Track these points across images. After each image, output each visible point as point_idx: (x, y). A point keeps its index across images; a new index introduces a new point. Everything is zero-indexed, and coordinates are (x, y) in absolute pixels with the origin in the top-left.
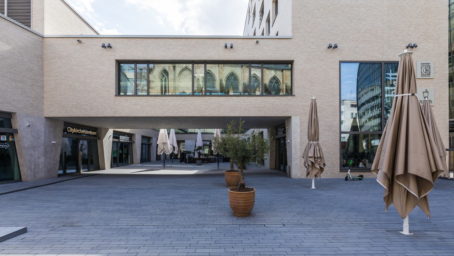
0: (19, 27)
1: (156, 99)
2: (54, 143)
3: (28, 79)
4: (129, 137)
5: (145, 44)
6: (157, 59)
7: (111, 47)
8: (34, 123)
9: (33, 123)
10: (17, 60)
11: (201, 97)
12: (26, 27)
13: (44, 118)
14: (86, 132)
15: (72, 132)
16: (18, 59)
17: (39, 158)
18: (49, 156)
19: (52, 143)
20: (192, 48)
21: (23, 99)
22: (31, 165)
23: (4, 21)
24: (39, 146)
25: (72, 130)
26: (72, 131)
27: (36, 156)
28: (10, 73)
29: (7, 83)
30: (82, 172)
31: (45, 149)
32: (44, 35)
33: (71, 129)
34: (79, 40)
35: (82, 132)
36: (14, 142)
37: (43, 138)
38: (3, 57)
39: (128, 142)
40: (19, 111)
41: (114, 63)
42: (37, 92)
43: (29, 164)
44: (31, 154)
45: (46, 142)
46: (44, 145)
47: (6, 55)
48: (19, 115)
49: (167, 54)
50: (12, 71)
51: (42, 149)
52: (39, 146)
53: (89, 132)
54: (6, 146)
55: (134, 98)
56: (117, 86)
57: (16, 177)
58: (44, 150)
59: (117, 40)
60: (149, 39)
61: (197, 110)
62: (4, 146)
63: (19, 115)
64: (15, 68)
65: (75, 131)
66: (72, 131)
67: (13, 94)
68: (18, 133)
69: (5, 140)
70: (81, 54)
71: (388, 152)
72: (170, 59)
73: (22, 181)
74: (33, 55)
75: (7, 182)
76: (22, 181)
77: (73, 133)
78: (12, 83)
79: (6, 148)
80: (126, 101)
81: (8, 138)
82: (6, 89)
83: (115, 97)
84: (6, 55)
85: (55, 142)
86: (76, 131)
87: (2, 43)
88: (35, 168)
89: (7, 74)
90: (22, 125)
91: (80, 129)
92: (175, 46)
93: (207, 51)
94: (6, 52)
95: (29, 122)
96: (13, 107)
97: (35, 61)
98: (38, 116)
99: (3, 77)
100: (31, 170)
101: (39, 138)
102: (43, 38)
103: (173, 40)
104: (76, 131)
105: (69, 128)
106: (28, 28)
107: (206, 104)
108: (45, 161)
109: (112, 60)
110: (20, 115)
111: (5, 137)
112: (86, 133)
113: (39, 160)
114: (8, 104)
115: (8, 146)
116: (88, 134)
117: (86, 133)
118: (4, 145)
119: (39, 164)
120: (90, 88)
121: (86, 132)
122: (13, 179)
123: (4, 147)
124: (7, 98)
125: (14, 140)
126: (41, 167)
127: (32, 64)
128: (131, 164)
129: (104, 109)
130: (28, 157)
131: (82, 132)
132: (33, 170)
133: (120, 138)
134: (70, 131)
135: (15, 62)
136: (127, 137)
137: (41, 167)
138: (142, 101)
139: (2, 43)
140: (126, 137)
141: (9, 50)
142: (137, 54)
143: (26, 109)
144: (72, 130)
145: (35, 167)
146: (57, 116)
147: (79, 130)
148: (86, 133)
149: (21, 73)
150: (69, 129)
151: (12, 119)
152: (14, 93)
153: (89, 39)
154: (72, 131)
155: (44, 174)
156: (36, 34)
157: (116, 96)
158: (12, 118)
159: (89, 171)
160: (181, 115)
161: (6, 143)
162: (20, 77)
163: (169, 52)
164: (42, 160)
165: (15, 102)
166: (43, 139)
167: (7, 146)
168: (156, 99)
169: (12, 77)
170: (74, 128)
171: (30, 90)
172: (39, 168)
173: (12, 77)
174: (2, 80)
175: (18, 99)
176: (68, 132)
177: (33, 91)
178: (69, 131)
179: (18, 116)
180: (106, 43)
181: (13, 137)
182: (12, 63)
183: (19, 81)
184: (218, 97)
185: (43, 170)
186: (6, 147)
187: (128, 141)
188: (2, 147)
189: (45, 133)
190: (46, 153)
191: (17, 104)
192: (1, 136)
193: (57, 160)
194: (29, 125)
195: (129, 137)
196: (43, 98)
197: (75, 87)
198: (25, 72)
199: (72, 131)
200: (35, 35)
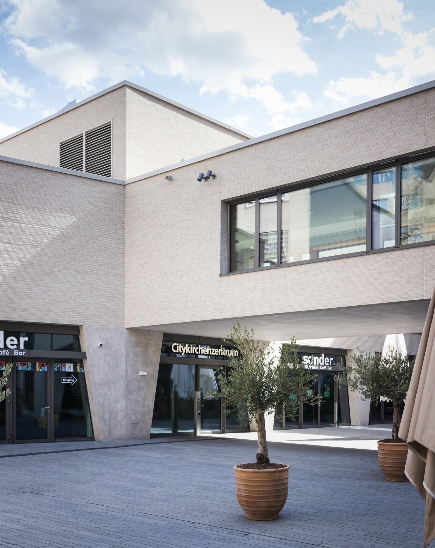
0: (87, 179)
1: (289, 272)
2: (144, 376)
3: (100, 266)
4: (331, 359)
5: (270, 153)
6: (292, 182)
7: (214, 176)
8: (109, 340)
9: (107, 341)
10: (84, 236)
11: (380, 254)
12: (101, 177)
13: (125, 330)
14: (212, 351)
15: (182, 352)
16: (86, 234)
17: (116, 402)
18: (134, 398)
19: (140, 374)
20: (362, 134)
21: (94, 302)
22: (104, 412)
23: (66, 178)
24: (118, 380)
25: (181, 348)
26: (181, 352)
27: (112, 398)
28: (74, 261)
29: (70, 279)
30: (200, 433)
31: (127, 386)
32: (125, 180)
33: (180, 347)
34: (167, 177)
35: (204, 351)
36: (84, 373)
37: (123, 367)
38: (65, 237)
39: (329, 371)
40: (88, 321)
41: (218, 208)
42: (114, 285)
43: (101, 412)
44: (105, 394)
45: (129, 373)
46: (125, 378)
47: (69, 232)
48: (86, 329)
49: (311, 164)
50: (78, 256)
51: (121, 386)
52: (118, 380)
53: (227, 351)
54: (72, 381)
55: (251, 276)
56: (227, 254)
57: (89, 435)
58: (125, 388)
59: (224, 158)
60: (277, 139)
61: (371, 290)
62: (70, 380)
63: (86, 329)
64: (81, 251)
65: (188, 350)
66: (182, 350)
67: (79, 295)
68: (86, 359)
69: (72, 370)
70: (172, 202)
71: (413, 390)
72: (316, 174)
73: (94, 440)
74: (109, 222)
75: (74, 438)
76: (94, 440)
77: (183, 354)
78: (77, 277)
79: (72, 385)
80: (237, 284)
81: (75, 368)
82: (69, 289)
83: (219, 278)
84: (69, 232)
85: (145, 373)
86: (190, 349)
87: (63, 215)
88: (110, 419)
89: (71, 263)
90: (91, 345)
91: (199, 346)
92: (327, 140)
93: (396, 133)
94: (69, 228)
95: (102, 339)
96: (79, 316)
97: (112, 231)
98: (116, 327)
99: (65, 269)
100: (105, 421)
101: (118, 367)
102: (124, 185)
103: (322, 128)
104: (190, 349)
105: (175, 344)
106: (105, 178)
107: (393, 271)
108: (126, 408)
109: (217, 203)
110: (89, 328)
111: (72, 365)
112: (213, 354)
113: (118, 405)
114: (71, 312)
115: (75, 380)
116: (217, 354)
117: (214, 352)
118: (69, 379)
119: (116, 413)
120: (184, 266)
121: (212, 351)
122: (86, 436)
123: (69, 382)
124: (70, 303)
125: (84, 370)
126: (120, 418)
127: (106, 238)
128: (340, 421)
129: (204, 305)
130: (100, 399)
131: (204, 351)
132: (107, 421)
133: (303, 361)
134: (178, 351)
135: (81, 242)
136: (325, 357)
137: (120, 418)
138: (264, 280)
139: (63, 215)
140: (321, 358)
141: (74, 223)
142: (255, 179)
143: (97, 317)
144: (181, 348)
145: (110, 417)
146: (141, 326)
147: (197, 348)
148: (214, 352)
149: (90, 258)
150: (175, 348)
151: (80, 336)
152: (80, 294)
153: (183, 169)
154: (182, 350)
155: (125, 429)
156: (112, 183)
157: (221, 275)
158: (80, 334)
159: (223, 432)
160: (337, 304)
161: (72, 375)
162: (88, 265)
163: (315, 158)
164: (121, 405)
165: (81, 308)
166: (124, 368)
167: (73, 380)
168: (289, 272)
169: (78, 268)
170: (187, 345)
171: (104, 283)
172: (116, 418)
173: (77, 266)
174: (64, 274)
175: (86, 303)
176: (174, 353)
177: (108, 284)
178: (175, 351)
179: (85, 330)
180: (204, 170)
181: (82, 366)
182: (78, 243)
183: (87, 271)
184: (421, 249)
185: (124, 423)
186: (73, 382)
187: (330, 368)
188: (67, 382)
189: (127, 357)
190: (128, 392)
191: (84, 310)
192: (66, 364)
193: (148, 406)
194: (101, 345)
195: (331, 359)
196: (124, 294)
197: (164, 267)
198: (96, 253)
199: (181, 352)
200: (111, 185)
